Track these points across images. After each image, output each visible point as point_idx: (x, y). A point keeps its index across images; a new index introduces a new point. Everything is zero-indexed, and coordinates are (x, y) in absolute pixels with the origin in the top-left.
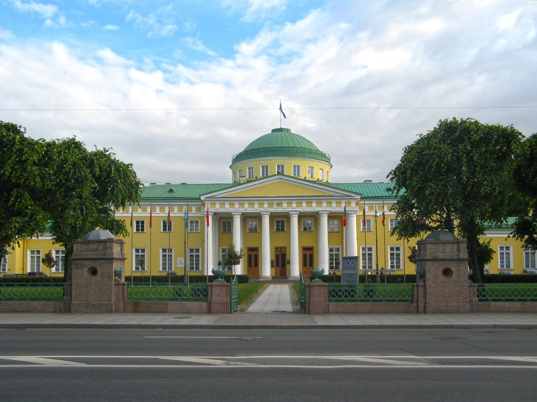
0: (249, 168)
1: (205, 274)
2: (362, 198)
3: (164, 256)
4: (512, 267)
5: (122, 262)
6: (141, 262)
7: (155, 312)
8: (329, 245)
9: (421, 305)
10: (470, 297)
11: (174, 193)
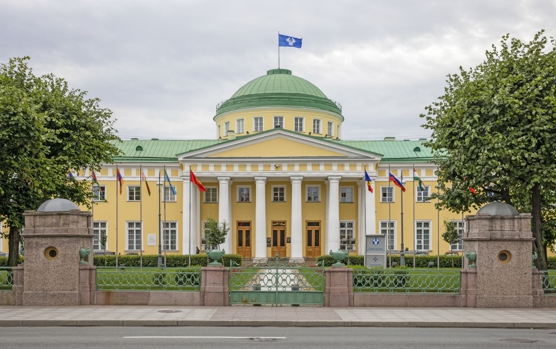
5: (89, 240)
7: (129, 305)
9: (471, 297)
10: (533, 287)
11: (143, 152)
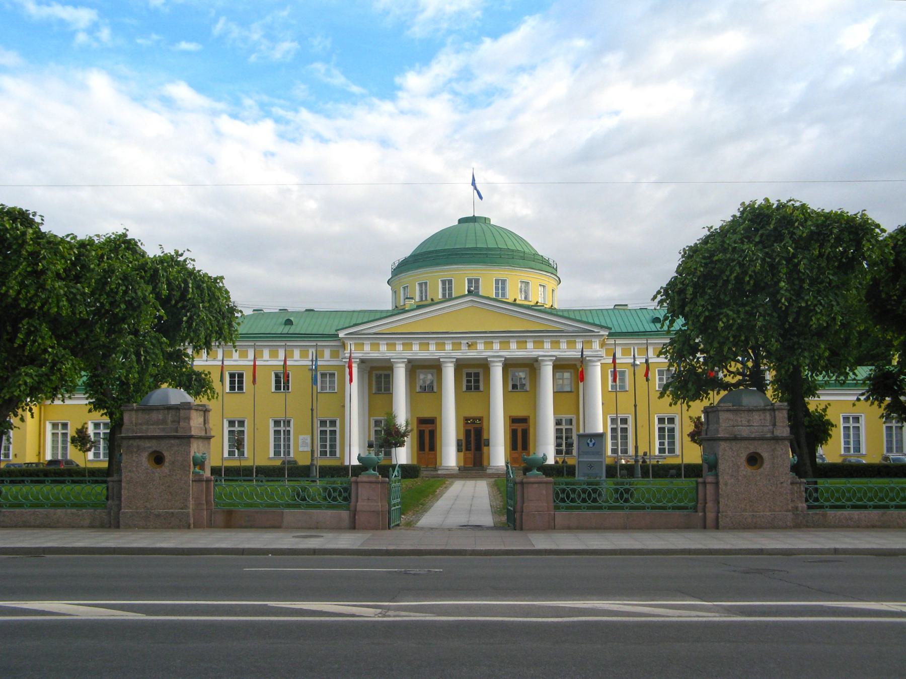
0: (421, 285)
1: (347, 463)
2: (611, 335)
3: (277, 432)
4: (863, 450)
5: (206, 442)
6: (237, 442)
7: (262, 528)
8: (554, 414)
9: (711, 515)
10: (793, 501)
11: (293, 327)
